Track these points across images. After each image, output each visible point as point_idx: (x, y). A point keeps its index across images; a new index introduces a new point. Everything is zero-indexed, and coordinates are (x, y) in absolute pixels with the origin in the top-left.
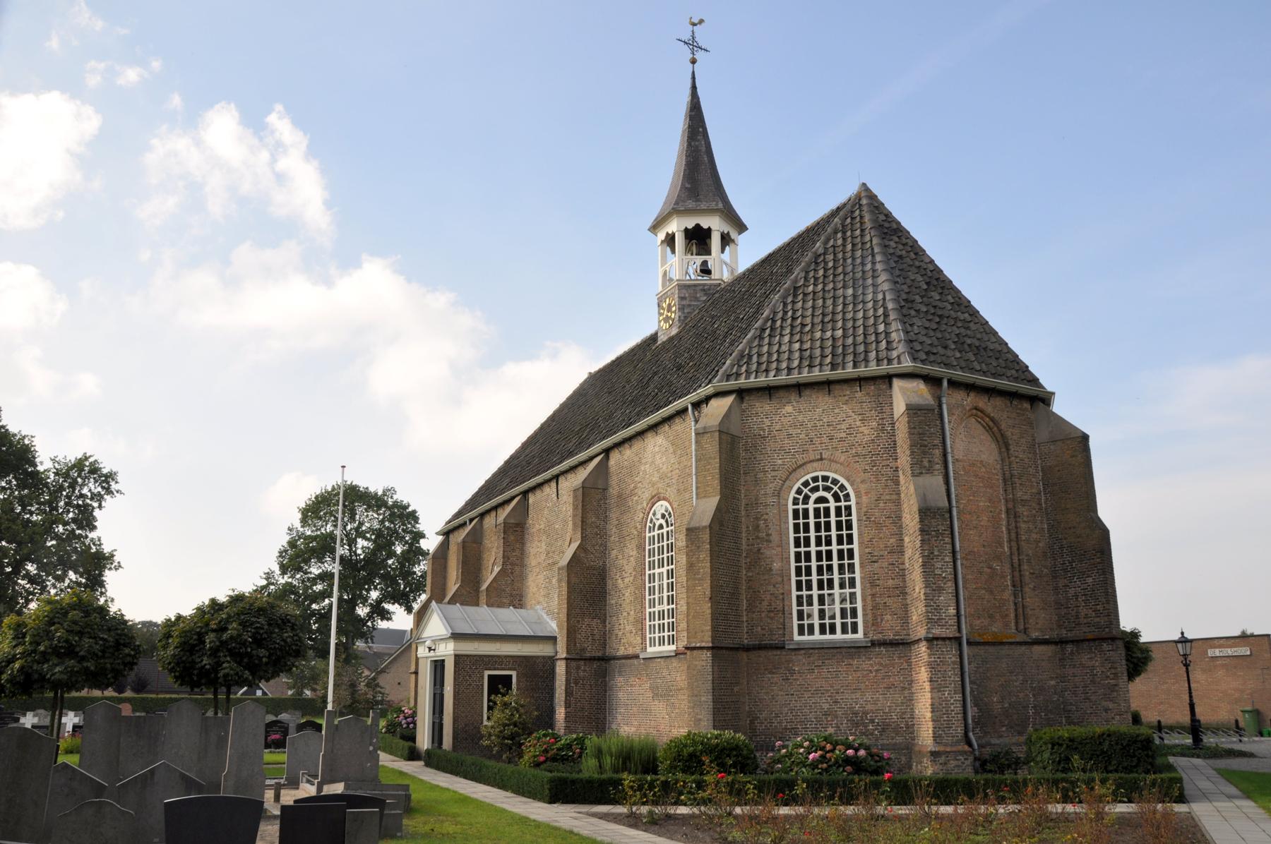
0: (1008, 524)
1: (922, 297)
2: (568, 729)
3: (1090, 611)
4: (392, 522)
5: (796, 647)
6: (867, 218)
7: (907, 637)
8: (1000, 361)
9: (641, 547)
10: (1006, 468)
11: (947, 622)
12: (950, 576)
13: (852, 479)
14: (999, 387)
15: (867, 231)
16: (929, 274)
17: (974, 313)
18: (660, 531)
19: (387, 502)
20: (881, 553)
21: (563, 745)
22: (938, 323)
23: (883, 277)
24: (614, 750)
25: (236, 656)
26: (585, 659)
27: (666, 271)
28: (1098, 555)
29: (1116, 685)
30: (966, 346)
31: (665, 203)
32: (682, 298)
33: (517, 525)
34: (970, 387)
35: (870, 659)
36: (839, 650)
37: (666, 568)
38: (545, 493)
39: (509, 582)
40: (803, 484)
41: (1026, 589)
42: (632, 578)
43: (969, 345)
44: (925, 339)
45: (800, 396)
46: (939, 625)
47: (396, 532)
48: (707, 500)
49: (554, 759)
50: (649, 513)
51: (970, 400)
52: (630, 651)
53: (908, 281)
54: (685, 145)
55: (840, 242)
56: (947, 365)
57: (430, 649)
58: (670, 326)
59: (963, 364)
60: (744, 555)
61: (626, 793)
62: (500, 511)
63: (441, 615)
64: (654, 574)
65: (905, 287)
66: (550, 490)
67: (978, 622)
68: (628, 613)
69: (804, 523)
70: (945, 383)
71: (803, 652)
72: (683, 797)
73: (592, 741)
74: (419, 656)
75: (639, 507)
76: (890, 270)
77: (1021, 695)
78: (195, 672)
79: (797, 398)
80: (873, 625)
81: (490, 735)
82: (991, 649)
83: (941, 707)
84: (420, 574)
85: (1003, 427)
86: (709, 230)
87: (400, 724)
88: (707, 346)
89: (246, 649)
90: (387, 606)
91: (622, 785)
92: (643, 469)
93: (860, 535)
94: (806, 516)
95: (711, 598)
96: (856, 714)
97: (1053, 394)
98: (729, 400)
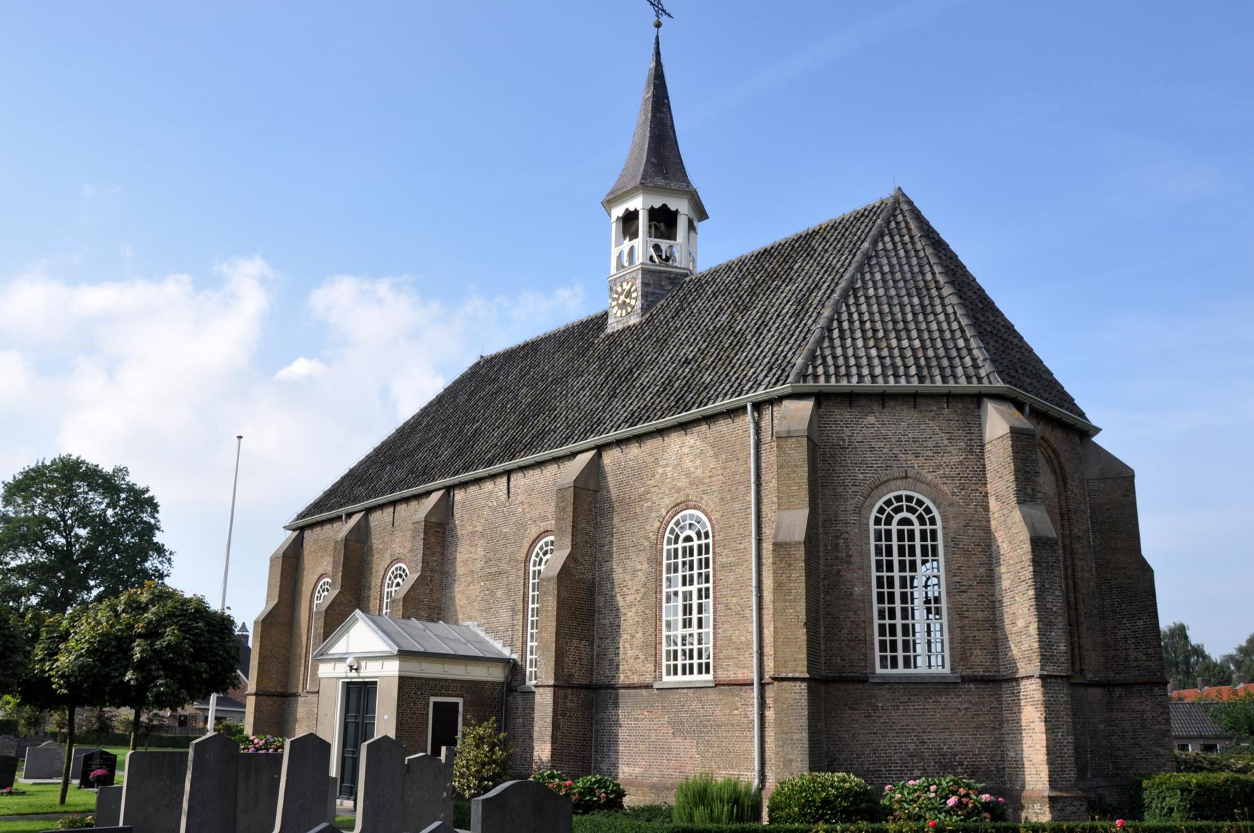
0: (1065, 561)
5: (881, 681)
7: (997, 674)
10: (1063, 502)
11: (1058, 659)
12: (1060, 611)
13: (938, 502)
20: (971, 583)
23: (947, 291)
25: (170, 669)
26: (573, 687)
32: (644, 284)
35: (959, 696)
36: (925, 686)
39: (427, 591)
41: (1083, 629)
42: (641, 595)
45: (884, 407)
48: (792, 512)
54: (649, 115)
58: (628, 314)
60: (822, 576)
63: (376, 628)
68: (633, 636)
70: (1027, 409)
71: (887, 686)
78: (108, 689)
79: (881, 409)
80: (962, 659)
83: (1054, 749)
89: (183, 660)
94: (889, 538)
95: (805, 624)
96: (944, 755)
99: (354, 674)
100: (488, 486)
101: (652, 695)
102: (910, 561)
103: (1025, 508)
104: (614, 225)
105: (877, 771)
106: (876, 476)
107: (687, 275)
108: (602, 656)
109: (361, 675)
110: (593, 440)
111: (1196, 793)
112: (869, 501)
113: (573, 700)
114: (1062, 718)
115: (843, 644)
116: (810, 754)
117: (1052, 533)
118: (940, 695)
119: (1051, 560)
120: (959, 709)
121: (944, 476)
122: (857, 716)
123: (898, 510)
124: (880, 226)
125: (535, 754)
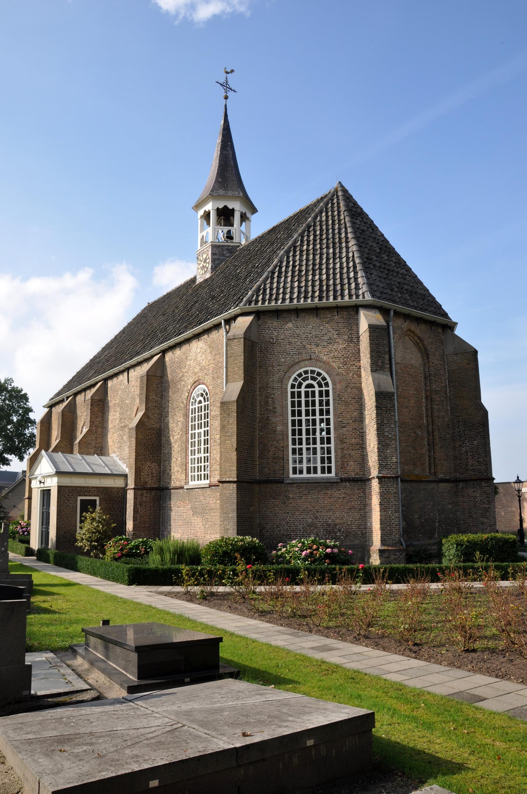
1: (377, 257)
2: (135, 535)
3: (475, 462)
4: (10, 400)
5: (292, 482)
6: (342, 204)
8: (425, 301)
9: (186, 416)
11: (391, 467)
13: (330, 373)
14: (425, 317)
15: (342, 213)
16: (381, 243)
17: (409, 270)
18: (200, 405)
19: (7, 388)
20: (348, 421)
21: (133, 546)
22: (387, 274)
23: (352, 242)
24: (172, 549)
26: (147, 489)
27: (203, 236)
28: (481, 426)
29: (489, 508)
30: (404, 291)
31: (204, 191)
32: (213, 254)
33: (100, 401)
34: (407, 317)
35: (339, 490)
36: (319, 484)
37: (203, 429)
38: (120, 380)
40: (298, 375)
42: (179, 436)
43: (406, 290)
44: (379, 283)
45: (298, 317)
46: (386, 469)
47: (13, 407)
49: (127, 555)
50: (192, 393)
51: (406, 325)
52: (178, 484)
53: (368, 246)
54: (219, 153)
55: (324, 218)
56: (393, 301)
57: (40, 482)
59: (403, 301)
61: (184, 579)
62: (88, 392)
64: (195, 433)
65: (366, 250)
66: (123, 378)
67: (406, 468)
68: (177, 459)
69: (298, 401)
70: (392, 313)
71: (295, 485)
72: (224, 581)
73: (156, 544)
74: (32, 487)
75: (185, 389)
76: (356, 238)
77: (432, 514)
79: (296, 319)
80: (342, 468)
81: (82, 539)
82: (415, 485)
84: (29, 435)
85: (425, 343)
86: (233, 210)
87: (18, 532)
88: (233, 284)
90: (6, 456)
91: (181, 573)
92: (188, 363)
93: (334, 409)
95: (236, 449)
96: (329, 525)
97: (457, 324)
98: (250, 319)
99: (42, 485)
100: (121, 377)
101: (184, 492)
102: (312, 410)
103: (376, 375)
104: (199, 220)
105: (288, 535)
106: (292, 359)
107: (239, 246)
108: (164, 471)
109: (46, 485)
110: (157, 349)
111: (466, 546)
112: (288, 374)
113: (147, 497)
114: (392, 502)
115: (270, 460)
116: (237, 525)
117: (391, 389)
118: (327, 490)
119: (389, 406)
120: (339, 498)
121: (334, 357)
122: (277, 503)
123: (305, 379)
124: (322, 206)
125: (127, 527)
